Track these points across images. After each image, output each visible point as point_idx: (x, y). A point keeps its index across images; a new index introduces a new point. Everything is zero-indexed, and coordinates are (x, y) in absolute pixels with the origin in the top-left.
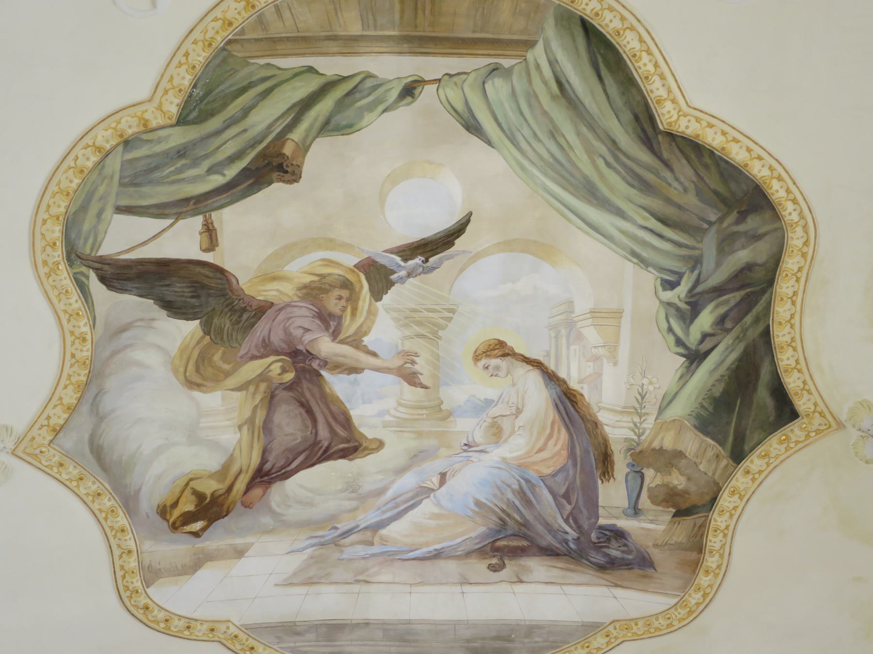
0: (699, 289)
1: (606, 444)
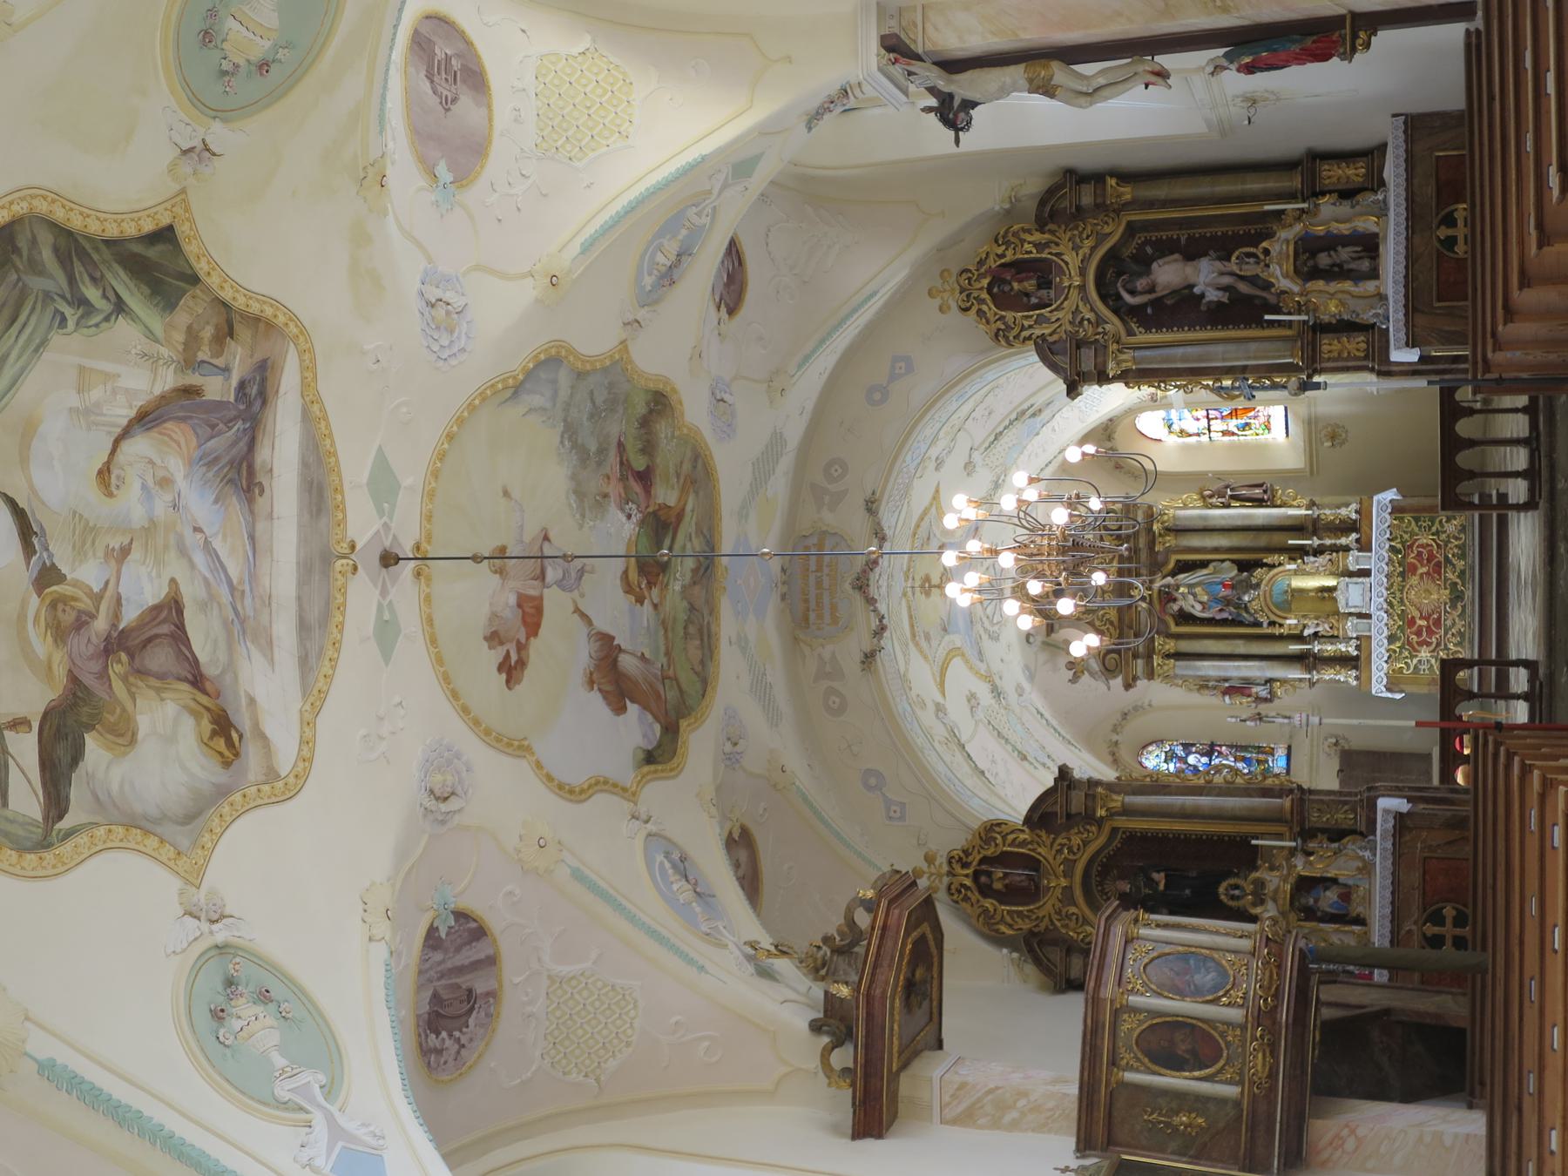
0: (68, 296)
1: (176, 390)
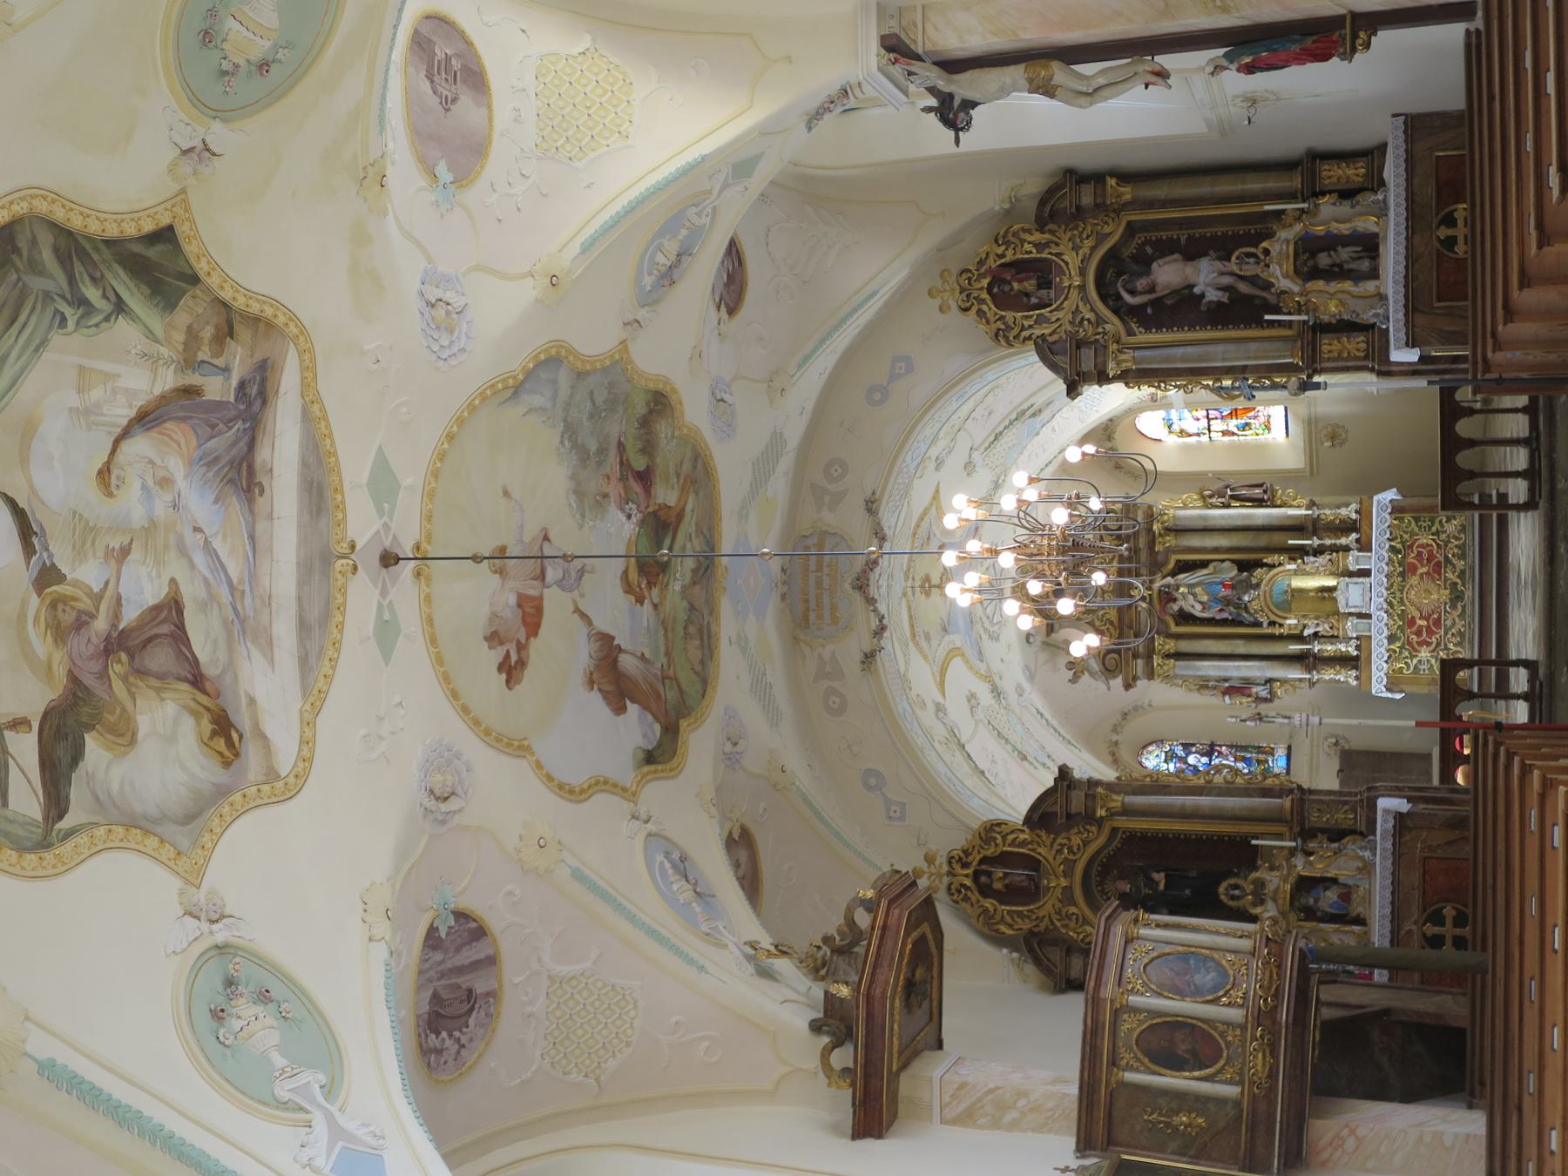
0: (68, 296)
1: (176, 390)
